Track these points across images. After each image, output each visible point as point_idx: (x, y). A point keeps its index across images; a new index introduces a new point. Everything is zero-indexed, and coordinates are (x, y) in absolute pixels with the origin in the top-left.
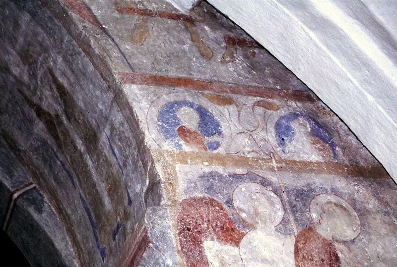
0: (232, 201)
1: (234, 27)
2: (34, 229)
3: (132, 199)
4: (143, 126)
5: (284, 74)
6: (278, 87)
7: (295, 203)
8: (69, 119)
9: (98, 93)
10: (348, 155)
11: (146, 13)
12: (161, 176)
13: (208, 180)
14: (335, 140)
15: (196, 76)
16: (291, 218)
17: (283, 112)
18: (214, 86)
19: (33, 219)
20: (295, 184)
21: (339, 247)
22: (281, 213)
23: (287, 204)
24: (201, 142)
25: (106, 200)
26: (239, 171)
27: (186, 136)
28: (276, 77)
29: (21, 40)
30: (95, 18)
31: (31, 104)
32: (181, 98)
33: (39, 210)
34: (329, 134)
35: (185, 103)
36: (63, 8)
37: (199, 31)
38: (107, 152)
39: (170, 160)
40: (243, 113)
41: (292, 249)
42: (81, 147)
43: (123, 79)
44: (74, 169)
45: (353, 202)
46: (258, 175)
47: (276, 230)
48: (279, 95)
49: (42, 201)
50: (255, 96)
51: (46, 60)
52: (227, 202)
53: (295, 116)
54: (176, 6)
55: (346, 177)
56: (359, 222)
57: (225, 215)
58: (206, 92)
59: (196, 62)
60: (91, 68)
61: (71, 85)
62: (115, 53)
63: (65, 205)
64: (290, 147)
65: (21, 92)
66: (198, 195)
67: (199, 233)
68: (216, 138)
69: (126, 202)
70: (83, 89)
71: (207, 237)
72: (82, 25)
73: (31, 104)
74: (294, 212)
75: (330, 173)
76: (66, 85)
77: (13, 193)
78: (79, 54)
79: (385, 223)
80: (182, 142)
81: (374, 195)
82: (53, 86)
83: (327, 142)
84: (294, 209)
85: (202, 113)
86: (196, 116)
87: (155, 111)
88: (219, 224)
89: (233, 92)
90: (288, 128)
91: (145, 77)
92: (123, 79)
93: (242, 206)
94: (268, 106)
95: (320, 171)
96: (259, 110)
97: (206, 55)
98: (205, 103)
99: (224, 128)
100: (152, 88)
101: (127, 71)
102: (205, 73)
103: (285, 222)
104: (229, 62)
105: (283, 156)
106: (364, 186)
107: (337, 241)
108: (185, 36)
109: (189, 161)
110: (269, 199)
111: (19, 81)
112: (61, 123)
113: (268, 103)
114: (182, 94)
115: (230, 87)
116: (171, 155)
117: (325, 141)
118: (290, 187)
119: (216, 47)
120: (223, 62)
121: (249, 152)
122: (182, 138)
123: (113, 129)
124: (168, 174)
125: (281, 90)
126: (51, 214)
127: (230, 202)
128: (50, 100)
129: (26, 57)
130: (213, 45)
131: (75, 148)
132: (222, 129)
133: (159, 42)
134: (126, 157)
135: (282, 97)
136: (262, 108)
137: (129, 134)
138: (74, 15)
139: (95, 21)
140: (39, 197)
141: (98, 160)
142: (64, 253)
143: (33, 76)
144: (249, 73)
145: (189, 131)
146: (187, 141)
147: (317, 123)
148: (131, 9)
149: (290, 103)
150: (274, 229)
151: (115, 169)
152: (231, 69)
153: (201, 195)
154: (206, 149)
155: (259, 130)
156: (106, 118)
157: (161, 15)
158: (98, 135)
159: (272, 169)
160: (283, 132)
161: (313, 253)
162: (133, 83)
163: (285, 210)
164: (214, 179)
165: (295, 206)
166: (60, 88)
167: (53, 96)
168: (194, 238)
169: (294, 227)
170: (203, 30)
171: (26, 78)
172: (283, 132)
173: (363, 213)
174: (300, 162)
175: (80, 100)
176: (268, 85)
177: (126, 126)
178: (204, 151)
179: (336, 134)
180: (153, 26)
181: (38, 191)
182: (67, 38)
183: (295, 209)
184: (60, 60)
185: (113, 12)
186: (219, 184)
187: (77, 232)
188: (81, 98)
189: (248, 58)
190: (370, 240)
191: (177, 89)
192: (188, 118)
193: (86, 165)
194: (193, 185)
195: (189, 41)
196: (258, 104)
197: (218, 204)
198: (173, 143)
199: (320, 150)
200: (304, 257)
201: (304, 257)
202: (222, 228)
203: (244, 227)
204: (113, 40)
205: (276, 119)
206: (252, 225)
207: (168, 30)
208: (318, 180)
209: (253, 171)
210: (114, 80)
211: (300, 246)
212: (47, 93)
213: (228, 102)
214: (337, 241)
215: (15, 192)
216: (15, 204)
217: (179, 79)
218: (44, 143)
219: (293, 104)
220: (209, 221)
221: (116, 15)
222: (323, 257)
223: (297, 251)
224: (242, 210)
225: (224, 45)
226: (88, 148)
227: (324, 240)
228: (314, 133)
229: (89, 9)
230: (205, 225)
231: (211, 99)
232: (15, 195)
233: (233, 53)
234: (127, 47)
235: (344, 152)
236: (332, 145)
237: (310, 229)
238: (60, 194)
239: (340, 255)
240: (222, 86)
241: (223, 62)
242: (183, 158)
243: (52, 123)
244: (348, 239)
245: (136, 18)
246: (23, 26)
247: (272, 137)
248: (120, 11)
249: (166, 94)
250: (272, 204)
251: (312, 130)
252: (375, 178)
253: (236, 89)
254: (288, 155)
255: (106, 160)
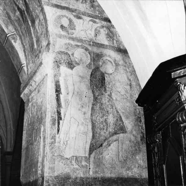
0: (74, 54)
2: (13, 47)
3: (42, 47)
7: (95, 58)
8: (27, 13)
9: (37, 6)
10: (118, 44)
12: (51, 42)
14: (115, 38)
15: (71, 7)
16: (92, 63)
18: (77, 11)
20: (97, 51)
22: (89, 61)
23: (92, 58)
24: (68, 32)
25: (35, 44)
26: (79, 44)
27: (63, 28)
28: (99, 11)
31: (16, 5)
32: (64, 14)
33: (15, 42)
34: (113, 35)
35: (65, 16)
40: (85, 23)
42: (30, 24)
43: (45, 3)
44: (27, 31)
46: (85, 46)
50: (90, 17)
52: (72, 54)
53: (103, 27)
55: (115, 52)
56: (115, 68)
58: (73, 13)
63: (24, 42)
66: (63, 50)
67: (60, 63)
68: (73, 31)
69: (40, 47)
70: (32, 4)
71: (62, 65)
73: (16, 5)
74: (94, 61)
77: (7, 34)
83: (111, 38)
85: (70, 21)
88: (67, 61)
89: (83, 15)
90: (99, 31)
91: (53, 4)
92: (45, 3)
93: (76, 57)
94: (95, 22)
96: (91, 23)
99: (77, 28)
103: (90, 64)
104: (84, 3)
105: (95, 41)
106: (120, 56)
109: (62, 38)
110: (86, 55)
112: (25, 14)
114: (65, 12)
117: (111, 37)
121: (84, 38)
122: (61, 29)
123: (40, 20)
125: (100, 16)
127: (73, 54)
128: (22, 5)
131: (28, 23)
134: (42, 31)
135: (100, 19)
136: (92, 22)
137: (44, 24)
140: (16, 37)
141: (34, 30)
144: (90, 8)
145: (64, 27)
147: (110, 30)
149: (102, 22)
150: (86, 66)
151: (39, 34)
154: (69, 34)
156: (38, 16)
158: (35, 21)
161: (97, 76)
165: (95, 59)
167: (23, 3)
168: (58, 65)
169: (93, 66)
173: (117, 65)
174: (100, 44)
175: (31, 7)
176: (96, 14)
177: (44, 21)
178: (68, 35)
179: (115, 36)
181: (16, 35)
183: (94, 60)
186: (70, 48)
187: (26, 51)
188: (31, 7)
189: (91, 3)
190: (117, 74)
191: (63, 10)
192: (65, 23)
193: (31, 31)
194: (62, 47)
196: (91, 20)
197: (69, 55)
199: (108, 41)
200: (93, 77)
201: (93, 77)
202: (68, 63)
203: (76, 64)
205: (96, 27)
209: (83, 45)
210: (42, 3)
211: (93, 73)
213: (80, 18)
214: (106, 73)
216: (8, 38)
218: (19, 19)
219: (103, 22)
220: (64, 60)
222: (100, 78)
223: (91, 75)
224: (76, 58)
227: (102, 72)
228: (108, 34)
230: (63, 61)
231: (74, 16)
236: (113, 40)
237: (98, 68)
238: (23, 38)
239: (106, 78)
240: (80, 12)
242: (60, 36)
243: (22, 12)
250: (87, 57)
252: (124, 53)
253: (84, 14)
254: (97, 41)
255: (37, 31)
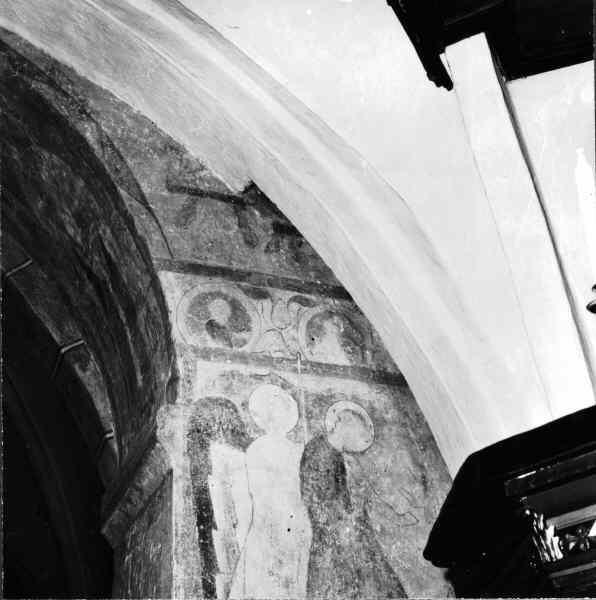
0: (247, 403)
1: (280, 214)
4: (172, 318)
5: (325, 272)
6: (319, 282)
11: (197, 193)
12: (182, 372)
13: (228, 379)
14: (368, 343)
15: (235, 266)
16: (305, 425)
17: (319, 310)
18: (252, 278)
19: (76, 375)
21: (347, 457)
25: (140, 377)
27: (213, 331)
28: (319, 271)
29: (76, 203)
30: (143, 196)
31: (85, 267)
33: (84, 370)
35: (219, 294)
36: (113, 184)
37: (248, 216)
38: (142, 329)
39: (192, 355)
41: (300, 457)
45: (372, 411)
47: (287, 437)
48: (318, 291)
49: (89, 359)
51: (96, 228)
52: (243, 405)
53: (330, 314)
54: (229, 187)
57: (238, 418)
58: (243, 284)
59: (240, 249)
60: (133, 247)
61: (117, 257)
62: (157, 237)
64: (318, 347)
65: (73, 250)
72: (130, 203)
74: (309, 419)
75: (354, 379)
76: (113, 256)
78: (125, 230)
79: (399, 435)
80: (208, 337)
81: (394, 405)
82: (102, 253)
84: (310, 416)
86: (228, 310)
87: (186, 302)
88: (230, 427)
89: (271, 285)
90: (320, 328)
94: (306, 303)
95: (345, 376)
96: (295, 306)
97: (251, 243)
98: (241, 296)
99: (254, 325)
100: (189, 277)
101: (166, 256)
102: (245, 263)
103: (297, 428)
107: (348, 452)
108: (233, 221)
111: (72, 240)
113: (307, 300)
114: (219, 284)
115: (269, 280)
116: (195, 351)
118: (310, 392)
119: (263, 234)
120: (267, 250)
123: (148, 311)
124: (189, 371)
126: (95, 374)
127: (245, 405)
128: (100, 266)
129: (81, 220)
130: (260, 232)
132: (252, 326)
133: (205, 225)
135: (321, 293)
138: (123, 192)
139: (143, 201)
142: (102, 414)
143: (85, 240)
144: (292, 264)
146: (213, 337)
147: (351, 323)
148: (182, 188)
152: (274, 260)
153: (218, 395)
155: (290, 328)
156: (145, 300)
157: (214, 195)
159: (295, 370)
160: (314, 331)
162: (170, 270)
163: (300, 415)
164: (234, 378)
165: (311, 412)
166: (108, 256)
168: (203, 440)
169: (306, 435)
170: (252, 214)
171: (79, 239)
172: (314, 331)
173: (379, 423)
174: (326, 365)
180: (201, 208)
182: (115, 212)
184: (108, 231)
185: (163, 191)
190: (381, 452)
192: (219, 312)
195: (236, 227)
196: (294, 299)
197: (233, 406)
198: (199, 338)
200: (309, 466)
201: (309, 466)
202: (233, 431)
203: (255, 431)
204: (157, 222)
206: (264, 431)
207: (216, 214)
208: (338, 385)
211: (308, 455)
212: (97, 258)
213: (262, 295)
215: (62, 347)
217: (217, 268)
218: (93, 304)
221: (165, 193)
223: (304, 460)
225: (271, 232)
226: (128, 320)
227: (334, 450)
229: (138, 186)
231: (247, 292)
232: (63, 350)
233: (279, 242)
234: (171, 230)
235: (373, 357)
236: (363, 348)
237: (322, 438)
239: (347, 466)
241: (267, 250)
243: (100, 288)
244: (359, 450)
245: (183, 199)
246: (79, 192)
247: (301, 335)
248: (171, 189)
249: (201, 284)
251: (345, 332)
